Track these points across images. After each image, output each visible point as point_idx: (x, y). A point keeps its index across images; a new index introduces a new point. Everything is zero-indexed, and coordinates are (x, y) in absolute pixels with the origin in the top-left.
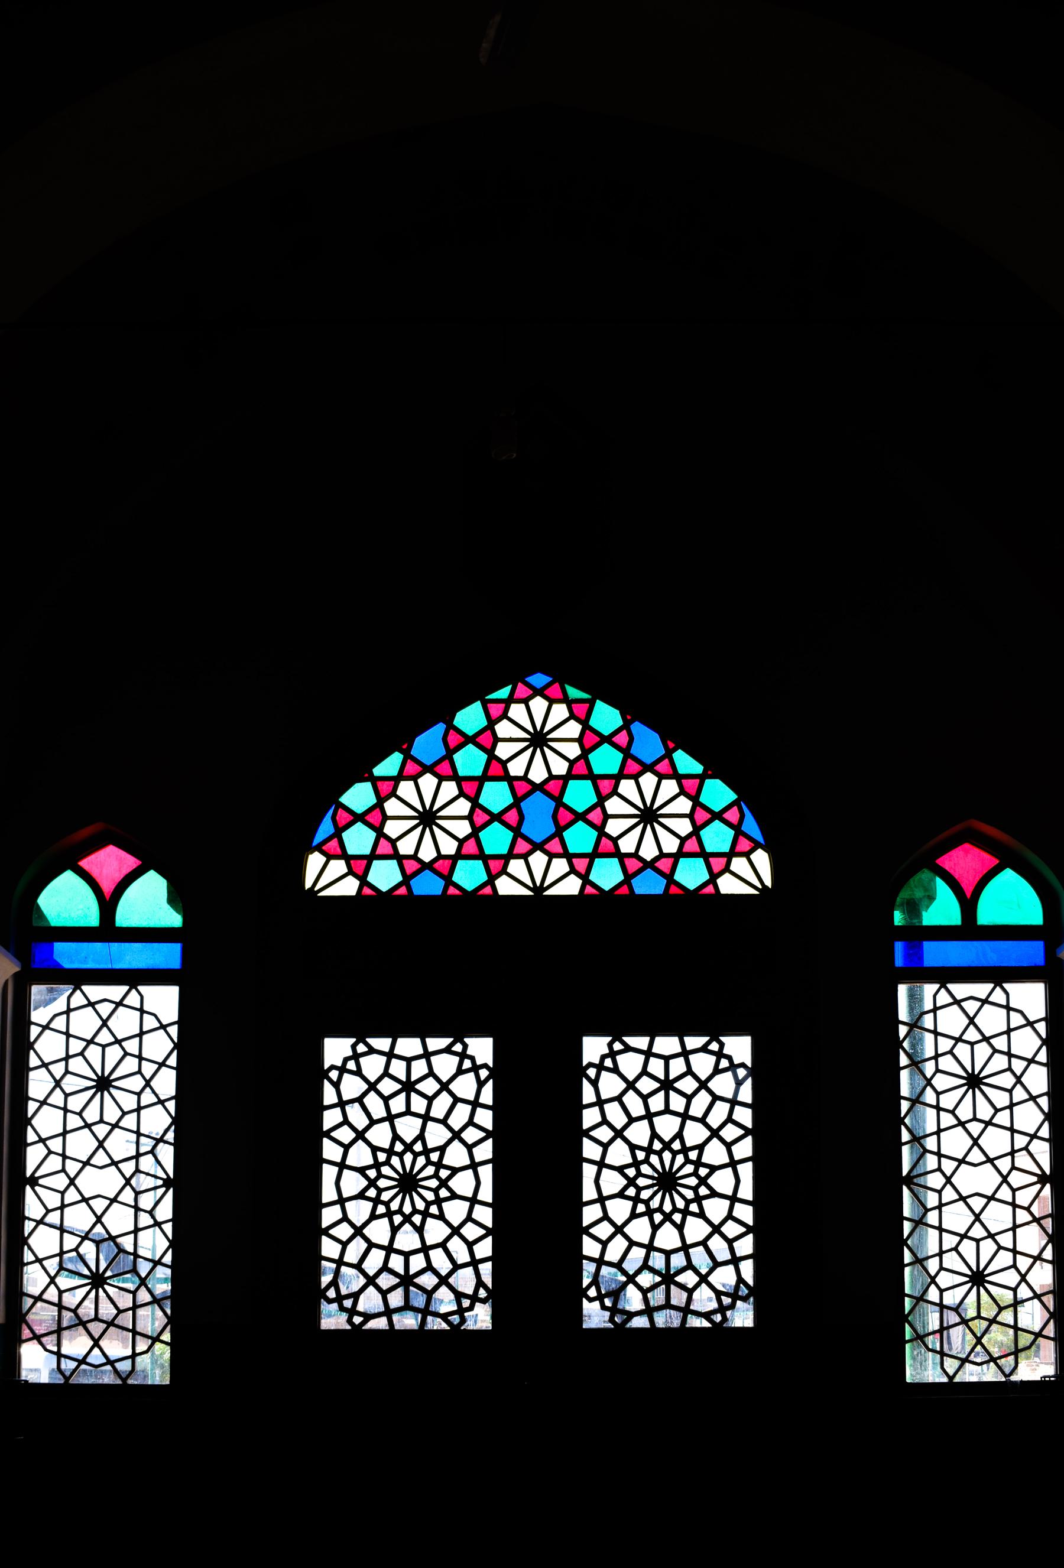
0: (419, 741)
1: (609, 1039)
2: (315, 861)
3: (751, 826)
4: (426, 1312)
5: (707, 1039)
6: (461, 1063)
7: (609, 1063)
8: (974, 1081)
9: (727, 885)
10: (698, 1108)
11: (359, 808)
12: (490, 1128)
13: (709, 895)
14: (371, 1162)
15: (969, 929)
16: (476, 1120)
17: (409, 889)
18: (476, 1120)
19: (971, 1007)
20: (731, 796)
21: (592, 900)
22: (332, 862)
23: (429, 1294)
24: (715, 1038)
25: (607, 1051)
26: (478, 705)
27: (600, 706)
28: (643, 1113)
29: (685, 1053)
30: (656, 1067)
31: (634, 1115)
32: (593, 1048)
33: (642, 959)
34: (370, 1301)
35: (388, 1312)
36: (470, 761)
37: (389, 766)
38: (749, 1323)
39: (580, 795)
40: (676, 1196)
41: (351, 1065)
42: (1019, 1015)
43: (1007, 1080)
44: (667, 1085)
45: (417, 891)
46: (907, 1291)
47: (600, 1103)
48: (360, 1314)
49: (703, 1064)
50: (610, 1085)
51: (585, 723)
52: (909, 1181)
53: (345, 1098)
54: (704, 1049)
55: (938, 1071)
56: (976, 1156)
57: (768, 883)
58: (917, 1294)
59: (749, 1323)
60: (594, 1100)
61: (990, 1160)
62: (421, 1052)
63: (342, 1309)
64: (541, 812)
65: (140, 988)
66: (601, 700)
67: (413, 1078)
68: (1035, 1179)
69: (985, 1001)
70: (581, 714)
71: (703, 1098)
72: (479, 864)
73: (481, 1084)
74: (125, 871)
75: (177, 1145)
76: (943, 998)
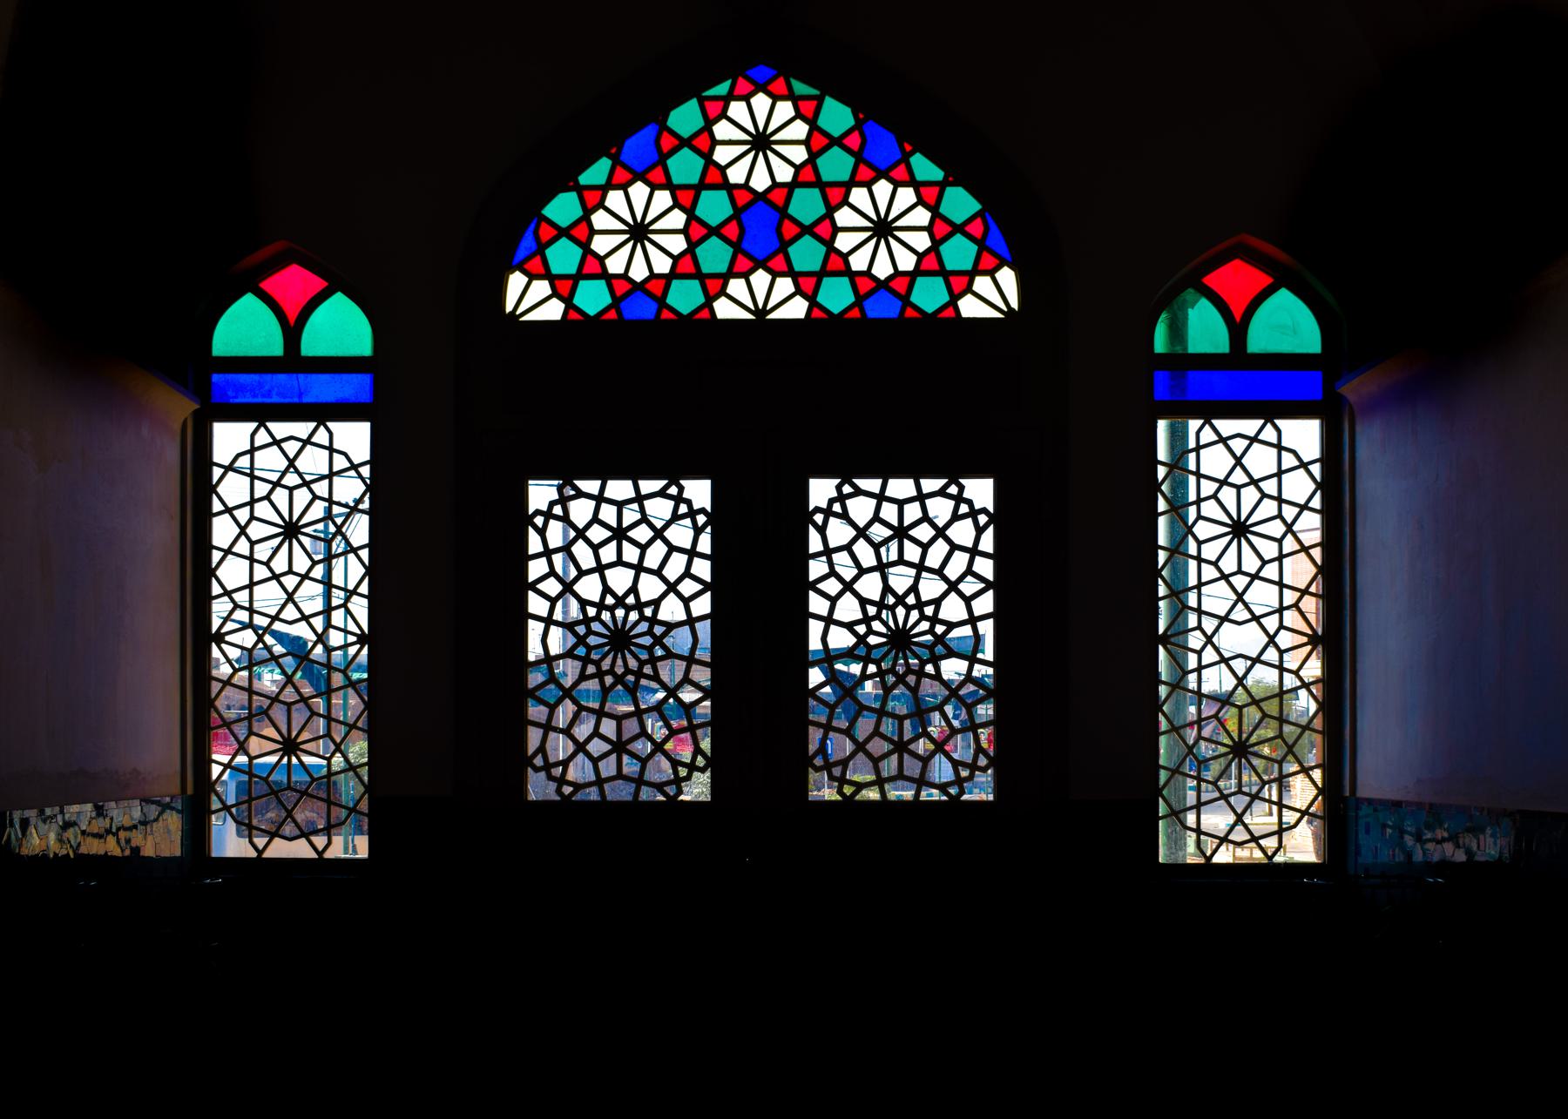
0: (630, 144)
1: (837, 481)
2: (516, 281)
3: (997, 240)
4: (922, 782)
5: (944, 481)
6: (956, 508)
7: (837, 509)
8: (1239, 529)
9: (970, 308)
10: (935, 558)
11: (564, 221)
12: (708, 579)
13: (949, 320)
14: (941, 616)
15: (293, 360)
16: (693, 571)
17: (862, 310)
18: (693, 571)
19: (1238, 445)
20: (974, 206)
21: (818, 323)
22: (535, 283)
23: (926, 760)
24: (953, 480)
25: (835, 494)
26: (694, 103)
27: (830, 104)
28: (544, 560)
29: (640, 499)
30: (608, 514)
31: (865, 565)
32: (699, 492)
33: (877, 389)
34: (579, 771)
35: (600, 782)
36: (685, 166)
37: (596, 173)
38: (814, 795)
39: (806, 206)
40: (628, 656)
41: (683, 509)
42: (1291, 456)
43: (1276, 529)
44: (901, 532)
45: (872, 314)
46: (1162, 762)
47: (828, 552)
48: (570, 783)
49: (941, 509)
50: (839, 533)
51: (812, 122)
52: (1165, 640)
53: (832, 545)
54: (942, 493)
55: (1199, 517)
56: (1240, 614)
57: (1015, 304)
58: (1172, 766)
59: (814, 795)
60: (541, 549)
61: (1256, 618)
62: (914, 493)
63: (550, 777)
64: (761, 229)
65: (329, 424)
66: (832, 96)
67: (895, 523)
68: (1305, 639)
69: (1254, 440)
70: (807, 112)
71: (940, 548)
72: (695, 284)
73: (980, 531)
74: (311, 294)
75: (371, 597)
76: (1208, 435)
